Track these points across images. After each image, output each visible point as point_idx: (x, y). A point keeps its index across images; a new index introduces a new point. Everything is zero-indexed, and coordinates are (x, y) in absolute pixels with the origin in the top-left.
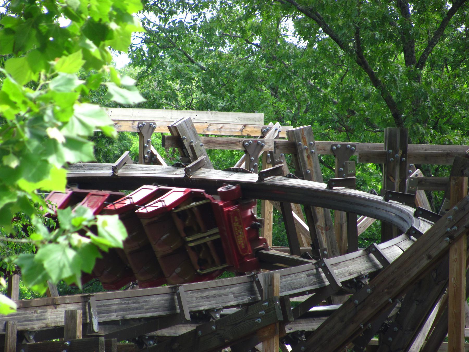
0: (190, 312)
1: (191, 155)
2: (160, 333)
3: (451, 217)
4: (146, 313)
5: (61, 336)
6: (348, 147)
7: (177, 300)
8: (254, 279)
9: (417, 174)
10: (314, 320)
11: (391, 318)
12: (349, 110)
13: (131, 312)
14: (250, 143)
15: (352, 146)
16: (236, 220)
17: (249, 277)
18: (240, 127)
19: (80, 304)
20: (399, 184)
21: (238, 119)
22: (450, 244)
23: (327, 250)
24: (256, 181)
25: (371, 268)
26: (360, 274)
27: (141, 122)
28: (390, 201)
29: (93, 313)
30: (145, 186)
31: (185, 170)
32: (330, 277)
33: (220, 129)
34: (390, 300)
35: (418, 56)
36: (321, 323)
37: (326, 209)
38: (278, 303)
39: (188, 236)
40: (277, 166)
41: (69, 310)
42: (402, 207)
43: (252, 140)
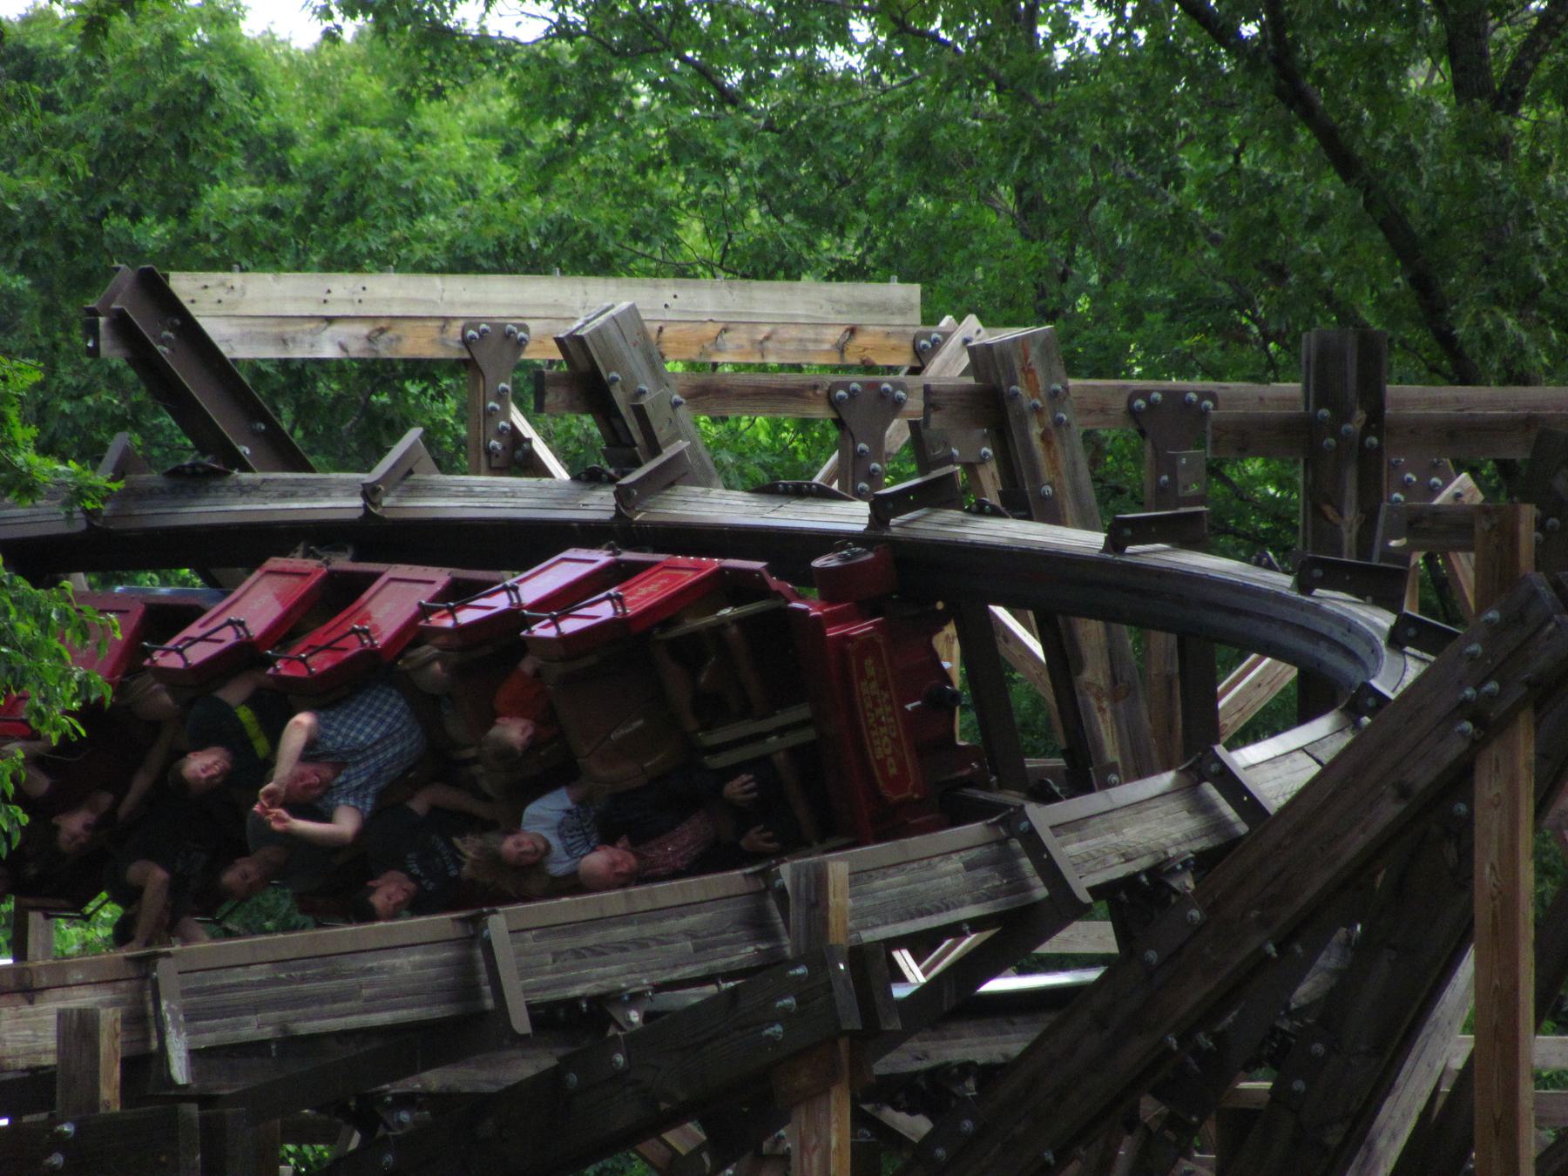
0: (531, 1007)
1: (638, 438)
2: (433, 1079)
3: (1475, 648)
4: (367, 1012)
5: (47, 1103)
6: (1190, 401)
7: (482, 965)
8: (767, 887)
9: (1458, 491)
10: (1013, 1024)
11: (1303, 1010)
12: (1264, 262)
13: (315, 1008)
14: (853, 394)
15: (1203, 395)
16: (871, 672)
17: (750, 874)
18: (834, 334)
19: (123, 985)
20: (1355, 529)
21: (828, 307)
22: (1477, 746)
23: (1121, 771)
24: (861, 528)
25: (1205, 833)
26: (1163, 857)
27: (472, 322)
28: (1318, 592)
29: (169, 1017)
30: (570, 553)
31: (616, 493)
32: (1050, 870)
33: (761, 342)
34: (1271, 949)
35: (1499, 70)
36: (1036, 1034)
37: (1114, 626)
38: (842, 967)
39: (707, 728)
40: (937, 473)
41: (72, 1010)
42: (1354, 614)
43: (859, 383)
